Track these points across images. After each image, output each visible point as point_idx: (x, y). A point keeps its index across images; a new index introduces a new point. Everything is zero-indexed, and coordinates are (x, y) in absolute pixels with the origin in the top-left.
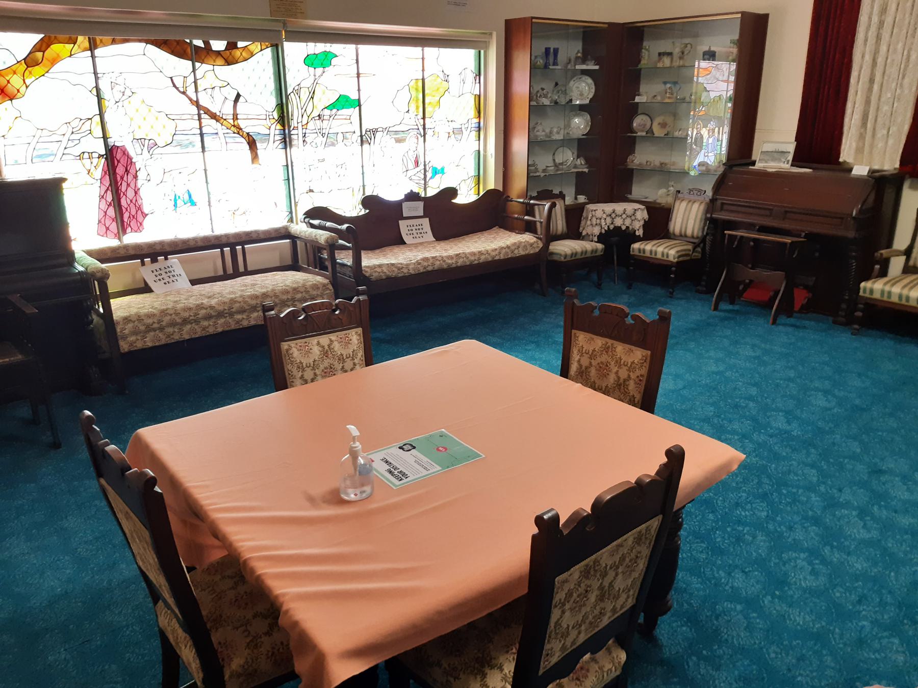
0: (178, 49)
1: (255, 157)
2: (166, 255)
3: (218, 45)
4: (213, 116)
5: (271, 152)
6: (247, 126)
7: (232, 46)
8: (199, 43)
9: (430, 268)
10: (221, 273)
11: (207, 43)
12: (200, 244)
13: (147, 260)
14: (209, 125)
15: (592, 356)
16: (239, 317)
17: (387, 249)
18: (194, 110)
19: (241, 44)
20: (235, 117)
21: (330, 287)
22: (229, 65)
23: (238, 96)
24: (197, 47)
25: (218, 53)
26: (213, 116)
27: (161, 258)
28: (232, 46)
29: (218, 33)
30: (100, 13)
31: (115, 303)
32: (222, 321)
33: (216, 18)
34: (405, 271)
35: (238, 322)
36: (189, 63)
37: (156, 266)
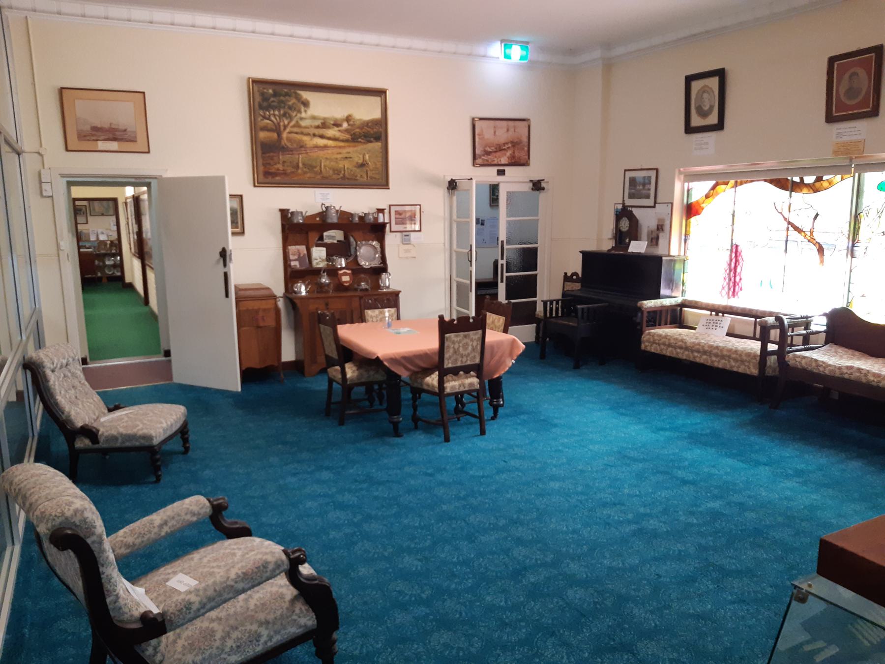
0: (782, 184)
1: (822, 261)
2: (724, 313)
3: (809, 179)
4: (796, 229)
5: (837, 257)
6: (818, 238)
7: (819, 179)
8: (797, 179)
9: (846, 376)
10: (752, 335)
11: (802, 179)
12: (739, 311)
13: (714, 313)
14: (793, 233)
15: (459, 342)
16: (696, 354)
17: (857, 353)
18: (785, 224)
19: (825, 178)
20: (812, 232)
21: (758, 359)
22: (814, 192)
23: (817, 215)
24: (793, 182)
25: (808, 185)
26: (796, 229)
27: (721, 314)
28: (819, 179)
29: (808, 170)
30: (740, 167)
31: (769, 345)
32: (687, 353)
33: (806, 162)
34: (821, 369)
35: (694, 357)
36: (788, 193)
37: (717, 318)
